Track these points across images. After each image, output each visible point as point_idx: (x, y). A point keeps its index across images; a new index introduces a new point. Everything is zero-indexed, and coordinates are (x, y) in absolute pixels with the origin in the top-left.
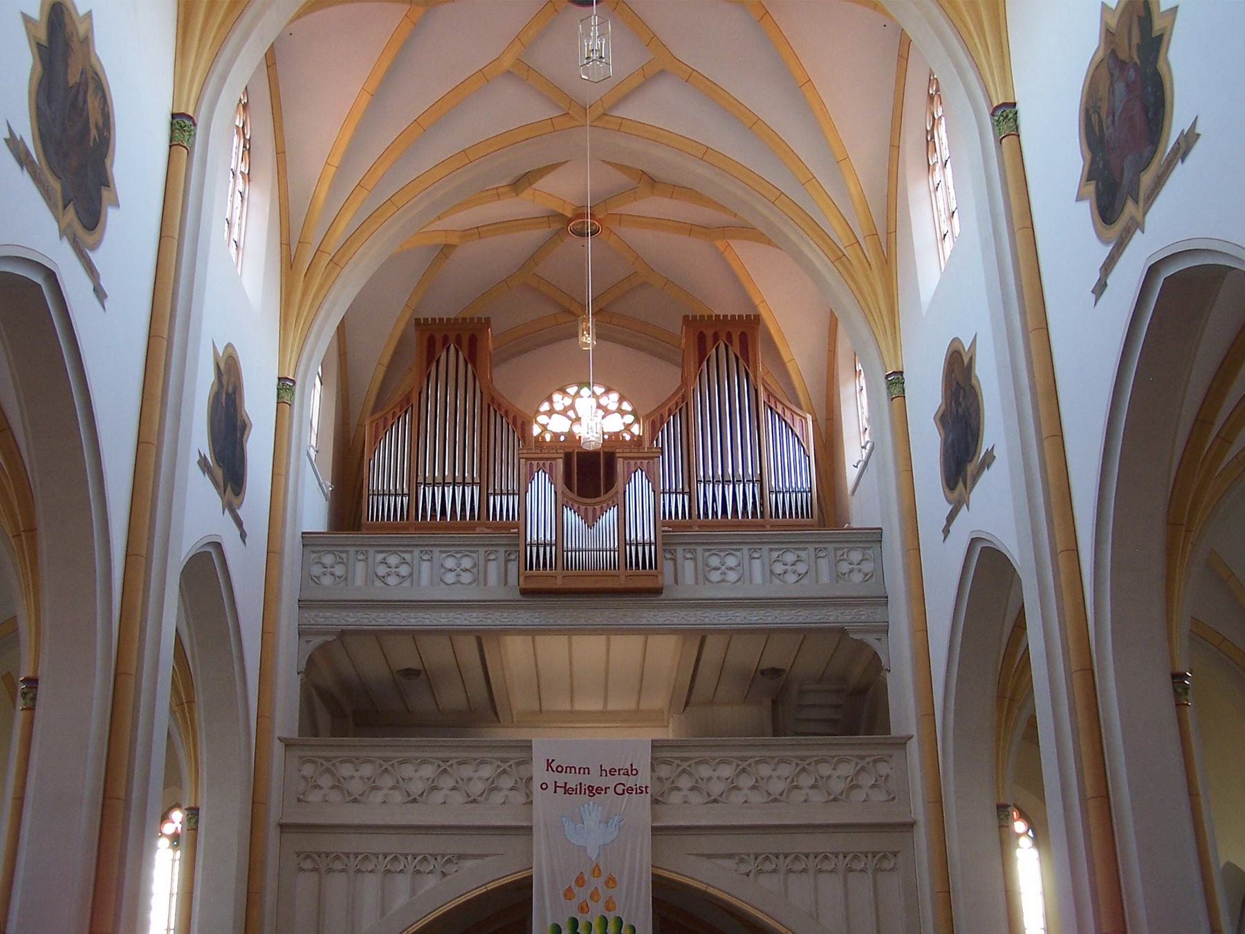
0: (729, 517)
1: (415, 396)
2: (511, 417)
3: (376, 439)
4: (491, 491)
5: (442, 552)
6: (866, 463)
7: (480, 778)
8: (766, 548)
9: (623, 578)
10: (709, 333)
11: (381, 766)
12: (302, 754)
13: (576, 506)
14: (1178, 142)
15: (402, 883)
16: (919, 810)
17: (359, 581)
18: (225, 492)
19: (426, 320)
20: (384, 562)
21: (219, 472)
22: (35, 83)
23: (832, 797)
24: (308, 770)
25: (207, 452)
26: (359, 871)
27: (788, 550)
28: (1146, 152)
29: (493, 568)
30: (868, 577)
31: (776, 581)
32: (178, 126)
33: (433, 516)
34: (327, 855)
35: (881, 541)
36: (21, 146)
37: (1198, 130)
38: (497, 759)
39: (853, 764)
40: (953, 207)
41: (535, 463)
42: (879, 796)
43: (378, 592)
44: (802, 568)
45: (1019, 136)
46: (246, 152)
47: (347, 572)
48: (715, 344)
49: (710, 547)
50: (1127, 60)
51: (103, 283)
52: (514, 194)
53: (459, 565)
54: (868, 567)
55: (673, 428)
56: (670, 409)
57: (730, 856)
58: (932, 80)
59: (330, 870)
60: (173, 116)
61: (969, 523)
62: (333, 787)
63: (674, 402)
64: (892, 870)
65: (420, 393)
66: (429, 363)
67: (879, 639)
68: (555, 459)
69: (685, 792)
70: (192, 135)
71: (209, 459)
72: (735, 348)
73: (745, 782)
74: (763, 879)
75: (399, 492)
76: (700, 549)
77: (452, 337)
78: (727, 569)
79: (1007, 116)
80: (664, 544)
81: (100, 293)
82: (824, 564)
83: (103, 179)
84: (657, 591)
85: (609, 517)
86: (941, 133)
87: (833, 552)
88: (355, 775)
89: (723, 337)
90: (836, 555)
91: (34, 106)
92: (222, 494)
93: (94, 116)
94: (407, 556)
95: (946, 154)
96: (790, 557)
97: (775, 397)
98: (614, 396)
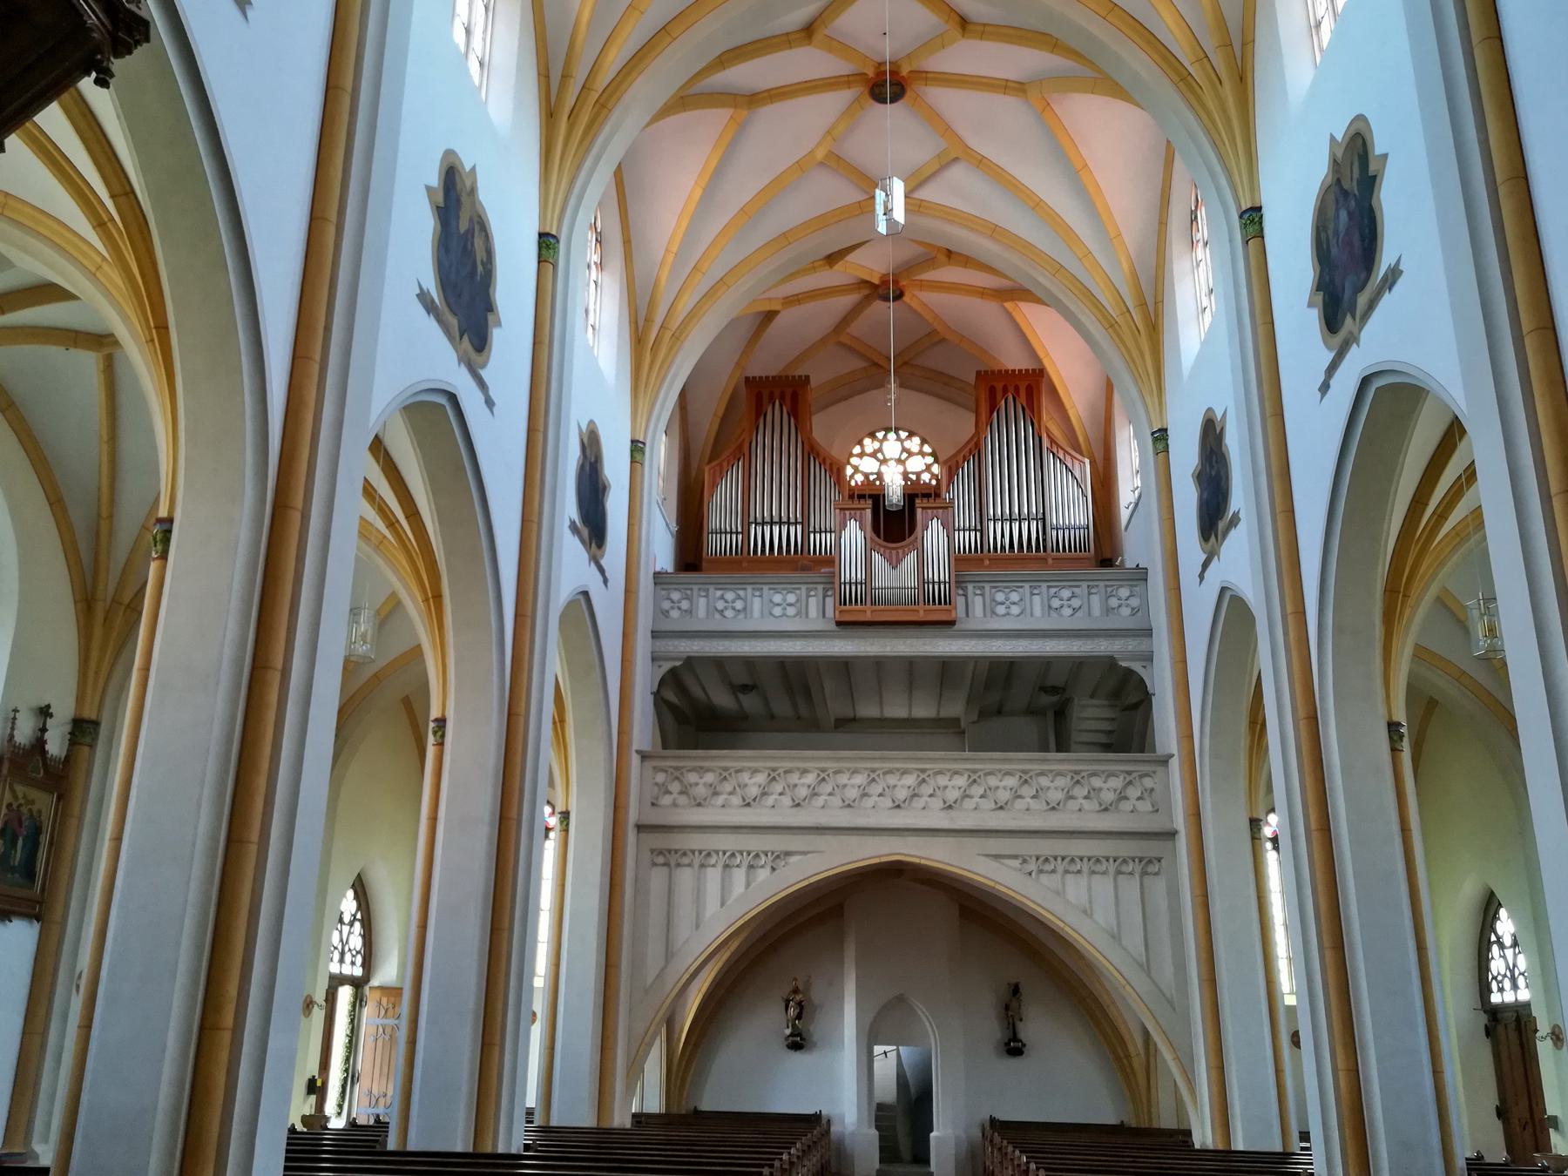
0: (1016, 551)
1: (746, 446)
3: (714, 485)
4: (811, 529)
5: (770, 589)
6: (1137, 505)
8: (1044, 585)
9: (922, 612)
10: (999, 387)
13: (882, 550)
14: (1386, 273)
16: (1180, 822)
17: (702, 612)
19: (754, 378)
20: (722, 597)
21: (585, 532)
22: (437, 237)
23: (1103, 807)
24: (660, 777)
27: (1064, 587)
28: (1363, 275)
29: (812, 601)
30: (1135, 611)
31: (1053, 614)
32: (544, 245)
33: (763, 551)
34: (676, 851)
35: (1146, 580)
36: (428, 297)
38: (817, 768)
39: (1122, 778)
40: (1211, 286)
41: (847, 513)
42: (1145, 806)
43: (716, 624)
44: (1076, 603)
45: (1263, 237)
46: (598, 245)
47: (692, 605)
48: (1003, 396)
50: (1349, 191)
51: (492, 393)
52: (827, 267)
53: (784, 600)
54: (1135, 602)
55: (967, 469)
56: (970, 449)
57: (1015, 857)
59: (678, 865)
60: (541, 235)
61: (1218, 573)
62: (681, 793)
63: (967, 449)
64: (1156, 874)
65: (751, 443)
66: (757, 419)
67: (1144, 667)
68: (864, 509)
70: (556, 251)
72: (1022, 399)
74: (1044, 878)
75: (734, 530)
76: (987, 586)
77: (777, 393)
78: (1011, 603)
79: (1253, 219)
81: (490, 403)
82: (1095, 600)
83: (489, 307)
84: (952, 623)
87: (1104, 590)
88: (701, 782)
89: (1011, 389)
90: (1106, 592)
91: (435, 259)
93: (480, 255)
94: (741, 593)
96: (1066, 593)
97: (1057, 444)
98: (916, 440)
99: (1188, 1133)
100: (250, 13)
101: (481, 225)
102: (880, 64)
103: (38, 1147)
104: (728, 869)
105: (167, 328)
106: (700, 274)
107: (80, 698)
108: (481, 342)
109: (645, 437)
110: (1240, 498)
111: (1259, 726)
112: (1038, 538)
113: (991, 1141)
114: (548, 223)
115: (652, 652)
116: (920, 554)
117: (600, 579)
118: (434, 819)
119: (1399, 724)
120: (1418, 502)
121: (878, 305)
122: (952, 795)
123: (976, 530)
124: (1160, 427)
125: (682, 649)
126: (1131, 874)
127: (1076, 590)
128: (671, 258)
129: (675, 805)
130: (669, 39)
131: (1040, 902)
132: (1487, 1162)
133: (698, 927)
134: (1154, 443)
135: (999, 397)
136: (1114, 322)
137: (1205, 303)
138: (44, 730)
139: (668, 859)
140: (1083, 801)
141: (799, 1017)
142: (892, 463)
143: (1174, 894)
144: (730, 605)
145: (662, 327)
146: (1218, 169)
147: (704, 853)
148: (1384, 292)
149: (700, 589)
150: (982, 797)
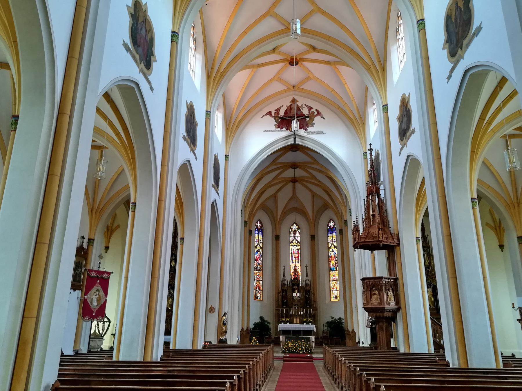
18: (191, 146)
21: (189, 140)
25: (185, 134)
37: (482, 26)
51: (152, 85)
58: (398, 11)
70: (210, 116)
71: (186, 136)
81: (151, 88)
83: (152, 54)
86: (401, 29)
92: (190, 146)
95: (403, 35)
100: (153, 91)
101: (150, 30)
103: (82, 348)
105: (17, 42)
107: (90, 233)
108: (148, 65)
109: (179, 30)
110: (415, 123)
111: (419, 205)
120: (423, 182)
124: (365, 152)
128: (236, 106)
130: (238, 58)
132: (504, 355)
134: (364, 156)
137: (402, 58)
138: (83, 242)
148: (475, 37)
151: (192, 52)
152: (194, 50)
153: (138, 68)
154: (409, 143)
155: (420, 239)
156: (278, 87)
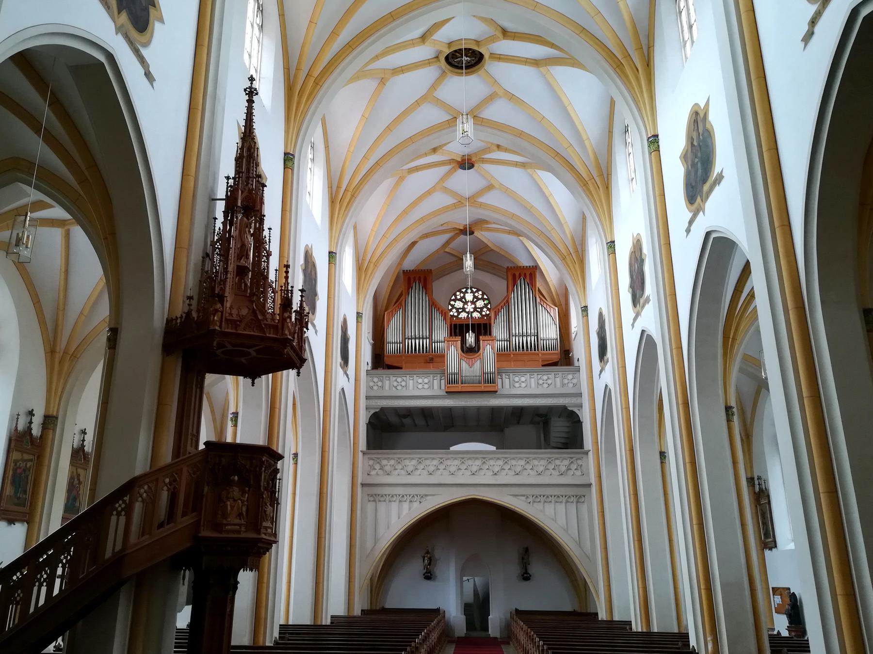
2: (440, 310)
3: (389, 321)
5: (417, 376)
7: (432, 465)
8: (536, 374)
9: (483, 387)
11: (397, 461)
12: (369, 456)
15: (406, 505)
16: (593, 480)
24: (371, 462)
26: (390, 501)
27: (544, 375)
29: (435, 382)
30: (575, 385)
31: (540, 387)
33: (412, 351)
34: (379, 495)
41: (450, 342)
42: (578, 473)
44: (549, 382)
45: (659, 151)
49: (515, 374)
55: (503, 312)
59: (380, 501)
60: (329, 253)
62: (380, 469)
67: (579, 410)
68: (457, 341)
69: (507, 470)
72: (528, 280)
73: (529, 467)
76: (511, 374)
80: (498, 373)
81: (148, 75)
82: (558, 380)
84: (497, 392)
85: (477, 364)
88: (388, 464)
89: (523, 275)
93: (313, 276)
94: (404, 378)
96: (545, 377)
99: (597, 614)
101: (314, 265)
102: (465, 225)
104: (401, 503)
106: (386, 239)
109: (336, 250)
110: (650, 289)
112: (535, 344)
113: (513, 619)
114: (332, 248)
115: (366, 405)
116: (482, 361)
117: (347, 379)
118: (294, 494)
119: (731, 407)
121: (462, 237)
122: (496, 469)
123: (507, 341)
125: (379, 404)
126: (572, 502)
127: (549, 376)
129: (377, 474)
131: (533, 515)
133: (388, 528)
135: (517, 279)
136: (586, 183)
138: (31, 423)
139: (375, 498)
140: (552, 471)
141: (429, 564)
142: (469, 304)
143: (590, 511)
144: (400, 383)
145: (345, 190)
146: (598, 223)
147: (390, 496)
149: (386, 377)
150: (509, 469)
151: (251, 33)
152: (311, 161)
153: (113, 24)
154: (710, 204)
155: (734, 410)
156: (441, 200)
